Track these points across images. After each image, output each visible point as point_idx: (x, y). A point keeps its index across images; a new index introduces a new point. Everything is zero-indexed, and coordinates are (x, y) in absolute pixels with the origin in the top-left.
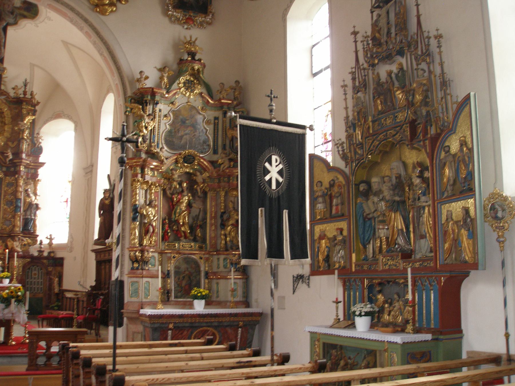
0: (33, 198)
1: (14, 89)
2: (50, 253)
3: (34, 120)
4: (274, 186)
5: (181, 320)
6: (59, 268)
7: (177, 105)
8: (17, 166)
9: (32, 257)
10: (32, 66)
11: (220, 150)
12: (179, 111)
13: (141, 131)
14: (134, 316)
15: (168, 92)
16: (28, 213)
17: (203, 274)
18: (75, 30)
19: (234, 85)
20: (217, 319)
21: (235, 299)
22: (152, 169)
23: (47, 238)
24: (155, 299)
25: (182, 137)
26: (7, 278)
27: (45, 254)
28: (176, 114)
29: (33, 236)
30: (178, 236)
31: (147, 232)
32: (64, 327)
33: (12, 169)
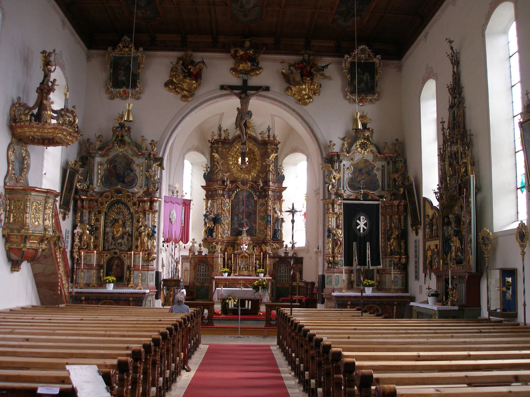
1: (261, 134)
3: (277, 157)
4: (362, 231)
5: (355, 299)
6: (299, 265)
7: (356, 160)
9: (280, 258)
11: (386, 188)
12: (358, 164)
13: (331, 181)
14: (329, 296)
15: (348, 153)
16: (276, 225)
19: (395, 142)
20: (379, 300)
21: (396, 288)
22: (339, 205)
23: (290, 243)
24: (343, 287)
25: (359, 181)
26: (262, 273)
28: (355, 166)
29: (281, 242)
31: (337, 244)
33: (263, 193)
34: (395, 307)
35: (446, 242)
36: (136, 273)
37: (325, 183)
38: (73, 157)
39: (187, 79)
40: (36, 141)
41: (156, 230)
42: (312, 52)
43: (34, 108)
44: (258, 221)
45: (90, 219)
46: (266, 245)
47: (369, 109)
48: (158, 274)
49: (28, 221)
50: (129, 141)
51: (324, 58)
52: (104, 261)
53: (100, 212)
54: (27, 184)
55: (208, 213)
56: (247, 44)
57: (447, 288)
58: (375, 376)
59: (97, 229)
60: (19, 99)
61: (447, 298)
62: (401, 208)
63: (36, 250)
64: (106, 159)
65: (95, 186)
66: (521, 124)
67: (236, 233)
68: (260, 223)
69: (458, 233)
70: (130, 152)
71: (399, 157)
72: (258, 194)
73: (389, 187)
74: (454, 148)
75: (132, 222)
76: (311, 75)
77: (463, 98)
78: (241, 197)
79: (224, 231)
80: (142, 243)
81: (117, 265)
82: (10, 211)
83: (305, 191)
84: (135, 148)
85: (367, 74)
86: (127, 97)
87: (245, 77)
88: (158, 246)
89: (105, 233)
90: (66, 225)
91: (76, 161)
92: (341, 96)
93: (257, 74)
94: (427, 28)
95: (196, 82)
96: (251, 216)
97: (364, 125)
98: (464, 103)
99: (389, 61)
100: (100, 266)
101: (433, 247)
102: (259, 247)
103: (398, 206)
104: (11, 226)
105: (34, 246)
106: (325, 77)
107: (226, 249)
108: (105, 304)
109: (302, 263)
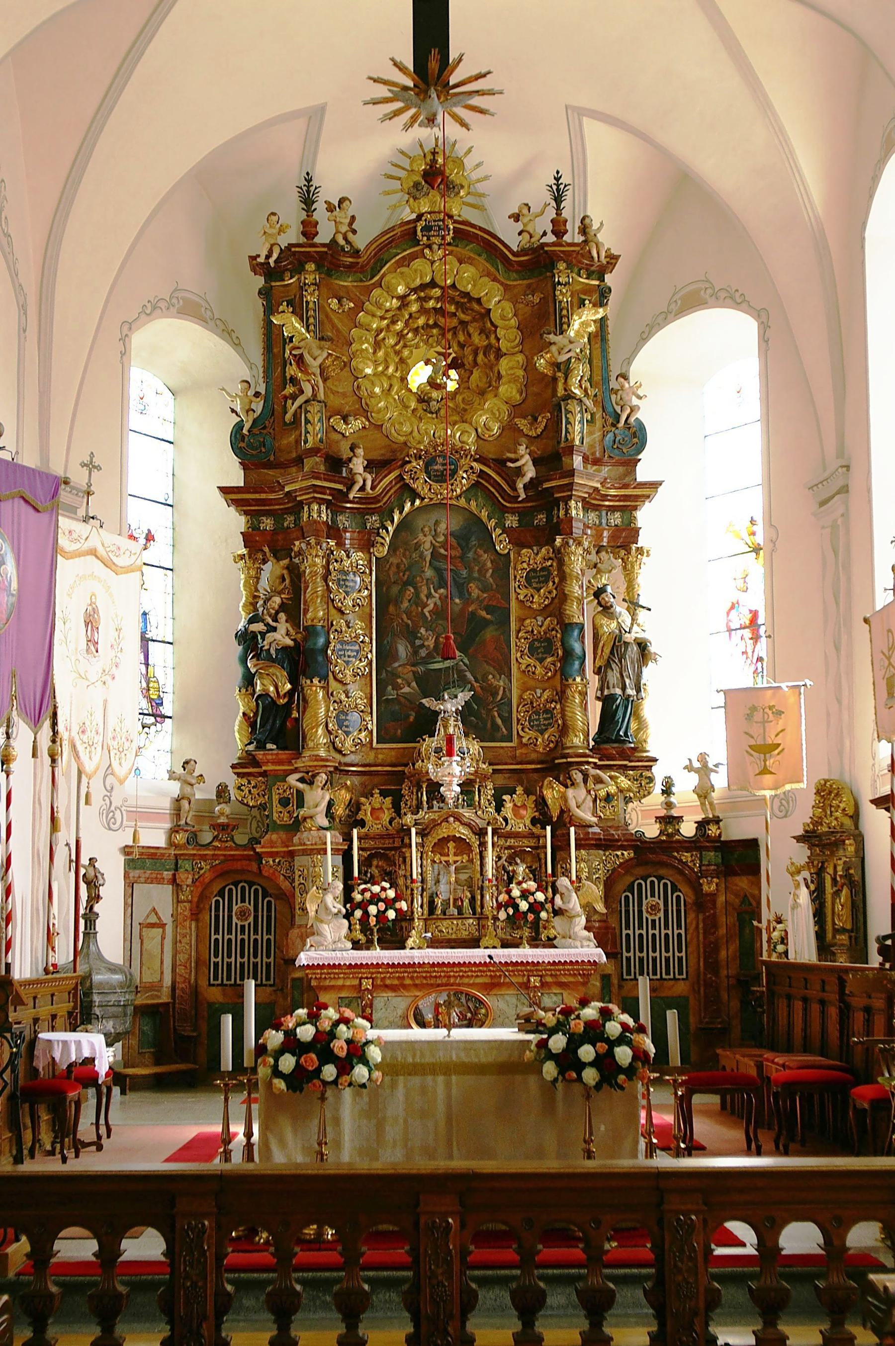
0: (626, 619)
1: (516, 217)
2: (702, 825)
3: (602, 323)
6: (742, 883)
8: (556, 502)
9: (639, 844)
10: (576, 114)
16: (613, 677)
18: (793, 143)
23: (689, 768)
27: (688, 829)
32: (769, 1154)
44: (520, 659)
46: (567, 783)
55: (258, 627)
67: (408, 723)
72: (512, 521)
78: (427, 543)
79: (343, 715)
96: (477, 634)
102: (528, 792)
107: (354, 807)
109: (753, 869)
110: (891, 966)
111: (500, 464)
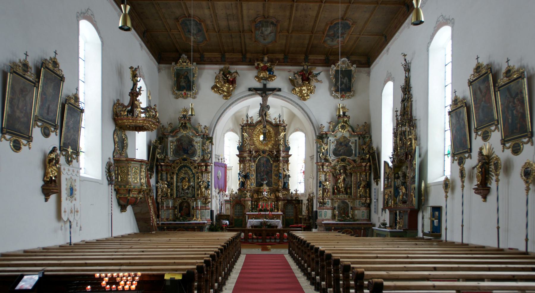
3: (285, 135)
9: (288, 200)
11: (357, 155)
12: (339, 139)
15: (333, 132)
17: (350, 208)
19: (364, 124)
27: (294, 198)
29: (288, 190)
30: (339, 192)
34: (362, 231)
35: (397, 189)
36: (198, 211)
37: (318, 152)
38: (154, 139)
39: (227, 83)
40: (131, 128)
41: (210, 184)
42: (309, 64)
43: (128, 106)
44: (274, 177)
45: (167, 178)
46: (279, 192)
47: (347, 102)
48: (212, 212)
49: (130, 180)
50: (190, 126)
51: (317, 68)
52: (177, 204)
53: (173, 173)
54: (127, 156)
56: (266, 59)
57: (396, 218)
58: (352, 266)
59: (172, 184)
60: (118, 100)
61: (396, 225)
62: (367, 168)
63: (136, 198)
64: (175, 138)
65: (169, 156)
66: (450, 113)
68: (274, 179)
69: (404, 184)
70: (191, 134)
71: (366, 133)
73: (359, 154)
74: (404, 129)
75: (194, 179)
76: (308, 80)
77: (411, 95)
78: (262, 162)
79: (252, 184)
80: (201, 192)
81: (186, 207)
82: (118, 174)
83: (304, 157)
84: (194, 131)
85: (346, 78)
86: (187, 97)
87: (265, 82)
88: (211, 194)
89: (177, 187)
90: (153, 181)
91: (156, 141)
92: (328, 93)
93: (273, 80)
94: (389, 44)
95: (233, 86)
96: (269, 173)
97: (344, 113)
98: (412, 98)
99: (361, 69)
100: (174, 208)
101: (389, 193)
103: (365, 166)
104: (119, 184)
105: (135, 196)
106: (318, 81)
108: (179, 230)
110: (92, 288)
111: (271, 152)
